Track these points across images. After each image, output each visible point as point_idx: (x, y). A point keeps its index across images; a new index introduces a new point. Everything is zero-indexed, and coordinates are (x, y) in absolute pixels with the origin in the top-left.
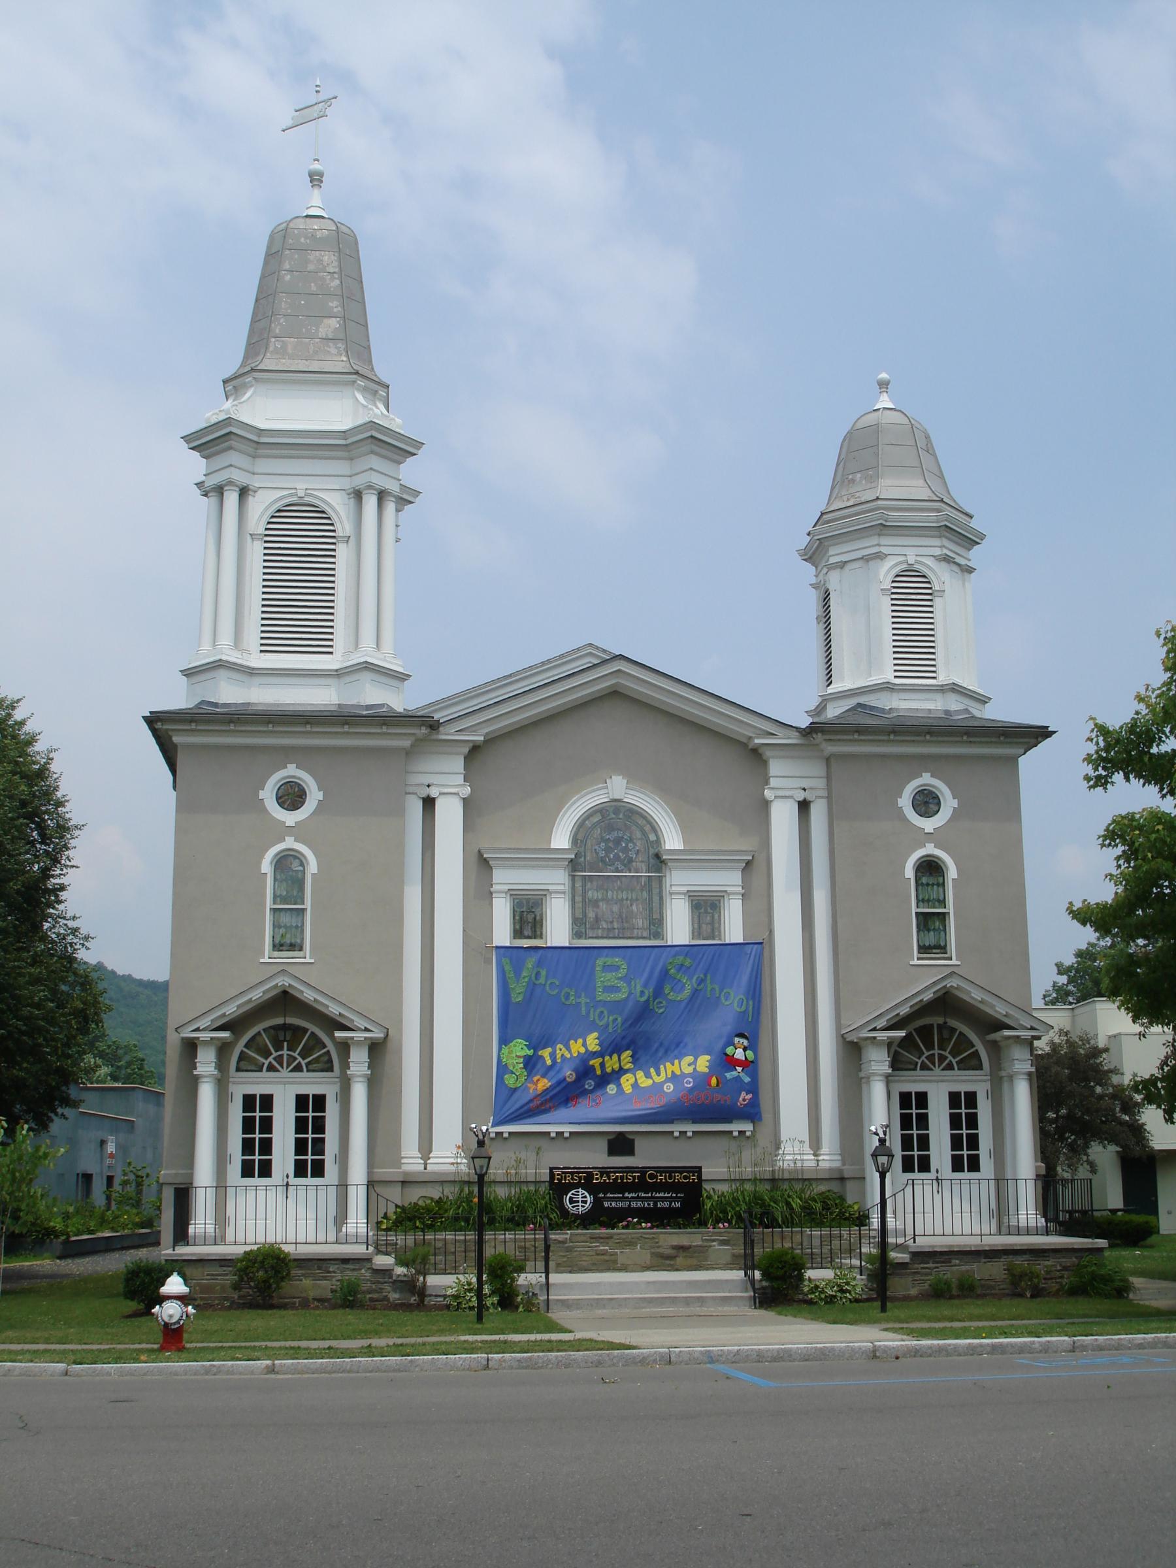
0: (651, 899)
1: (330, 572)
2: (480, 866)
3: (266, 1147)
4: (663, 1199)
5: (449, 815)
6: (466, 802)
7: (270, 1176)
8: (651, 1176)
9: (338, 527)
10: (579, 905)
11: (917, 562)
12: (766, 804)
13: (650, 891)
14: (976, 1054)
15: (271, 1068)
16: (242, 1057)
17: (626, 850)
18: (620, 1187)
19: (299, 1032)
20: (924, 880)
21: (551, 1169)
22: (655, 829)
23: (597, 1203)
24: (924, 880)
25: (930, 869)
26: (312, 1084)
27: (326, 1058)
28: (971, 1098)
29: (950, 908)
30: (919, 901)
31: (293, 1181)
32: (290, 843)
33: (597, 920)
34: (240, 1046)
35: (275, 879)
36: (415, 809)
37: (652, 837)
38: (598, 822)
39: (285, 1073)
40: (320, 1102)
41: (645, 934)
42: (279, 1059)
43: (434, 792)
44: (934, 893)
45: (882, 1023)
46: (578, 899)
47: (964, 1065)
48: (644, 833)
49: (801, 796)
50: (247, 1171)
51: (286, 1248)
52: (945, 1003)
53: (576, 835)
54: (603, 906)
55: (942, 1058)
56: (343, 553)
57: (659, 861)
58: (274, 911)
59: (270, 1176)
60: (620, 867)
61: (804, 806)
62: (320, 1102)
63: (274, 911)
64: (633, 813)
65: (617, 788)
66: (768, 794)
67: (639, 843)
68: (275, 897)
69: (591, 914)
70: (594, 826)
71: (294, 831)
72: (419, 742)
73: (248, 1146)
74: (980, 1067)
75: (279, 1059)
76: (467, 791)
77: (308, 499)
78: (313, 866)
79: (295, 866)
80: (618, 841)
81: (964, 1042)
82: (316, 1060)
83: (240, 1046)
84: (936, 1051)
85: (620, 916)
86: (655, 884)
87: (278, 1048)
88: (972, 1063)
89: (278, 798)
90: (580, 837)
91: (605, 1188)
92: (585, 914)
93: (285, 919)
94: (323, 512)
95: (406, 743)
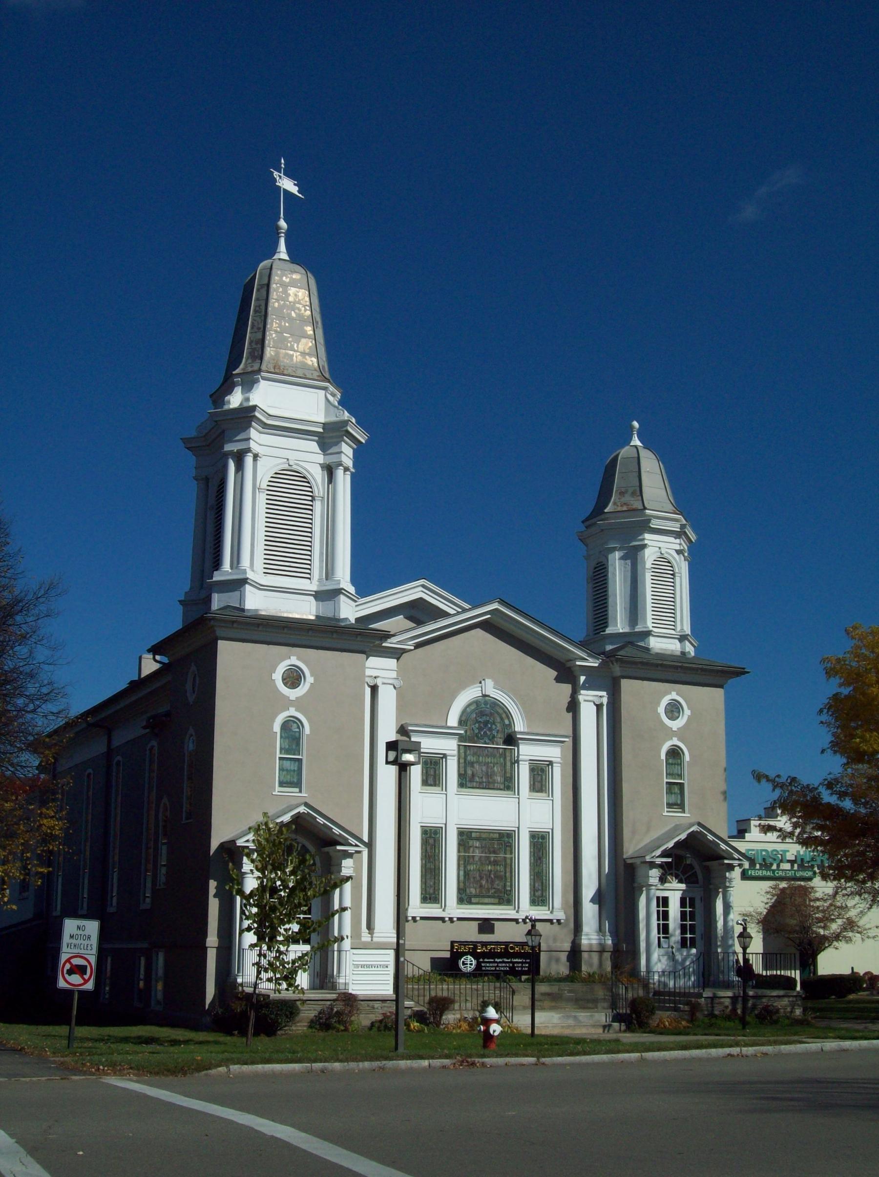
0: (505, 764)
4: (518, 963)
7: (432, 959)
8: (512, 948)
10: (462, 765)
11: (667, 553)
13: (505, 758)
17: (491, 729)
18: (492, 955)
20: (670, 761)
21: (452, 943)
22: (509, 715)
23: (479, 965)
24: (670, 761)
25: (292, 733)
29: (278, 755)
30: (669, 774)
32: (292, 712)
33: (473, 775)
35: (281, 737)
37: (507, 722)
38: (474, 710)
41: (502, 787)
44: (676, 769)
46: (462, 761)
48: (502, 719)
52: (301, 824)
53: (461, 716)
54: (477, 766)
57: (511, 740)
58: (280, 758)
59: (432, 959)
60: (487, 741)
63: (280, 758)
67: (498, 725)
68: (281, 749)
69: (469, 772)
70: (472, 712)
71: (298, 703)
74: (697, 882)
77: (295, 467)
78: (307, 730)
79: (294, 728)
80: (486, 723)
85: (487, 773)
86: (508, 754)
89: (283, 679)
90: (463, 718)
91: (484, 955)
92: (465, 771)
93: (287, 764)
94: (304, 477)
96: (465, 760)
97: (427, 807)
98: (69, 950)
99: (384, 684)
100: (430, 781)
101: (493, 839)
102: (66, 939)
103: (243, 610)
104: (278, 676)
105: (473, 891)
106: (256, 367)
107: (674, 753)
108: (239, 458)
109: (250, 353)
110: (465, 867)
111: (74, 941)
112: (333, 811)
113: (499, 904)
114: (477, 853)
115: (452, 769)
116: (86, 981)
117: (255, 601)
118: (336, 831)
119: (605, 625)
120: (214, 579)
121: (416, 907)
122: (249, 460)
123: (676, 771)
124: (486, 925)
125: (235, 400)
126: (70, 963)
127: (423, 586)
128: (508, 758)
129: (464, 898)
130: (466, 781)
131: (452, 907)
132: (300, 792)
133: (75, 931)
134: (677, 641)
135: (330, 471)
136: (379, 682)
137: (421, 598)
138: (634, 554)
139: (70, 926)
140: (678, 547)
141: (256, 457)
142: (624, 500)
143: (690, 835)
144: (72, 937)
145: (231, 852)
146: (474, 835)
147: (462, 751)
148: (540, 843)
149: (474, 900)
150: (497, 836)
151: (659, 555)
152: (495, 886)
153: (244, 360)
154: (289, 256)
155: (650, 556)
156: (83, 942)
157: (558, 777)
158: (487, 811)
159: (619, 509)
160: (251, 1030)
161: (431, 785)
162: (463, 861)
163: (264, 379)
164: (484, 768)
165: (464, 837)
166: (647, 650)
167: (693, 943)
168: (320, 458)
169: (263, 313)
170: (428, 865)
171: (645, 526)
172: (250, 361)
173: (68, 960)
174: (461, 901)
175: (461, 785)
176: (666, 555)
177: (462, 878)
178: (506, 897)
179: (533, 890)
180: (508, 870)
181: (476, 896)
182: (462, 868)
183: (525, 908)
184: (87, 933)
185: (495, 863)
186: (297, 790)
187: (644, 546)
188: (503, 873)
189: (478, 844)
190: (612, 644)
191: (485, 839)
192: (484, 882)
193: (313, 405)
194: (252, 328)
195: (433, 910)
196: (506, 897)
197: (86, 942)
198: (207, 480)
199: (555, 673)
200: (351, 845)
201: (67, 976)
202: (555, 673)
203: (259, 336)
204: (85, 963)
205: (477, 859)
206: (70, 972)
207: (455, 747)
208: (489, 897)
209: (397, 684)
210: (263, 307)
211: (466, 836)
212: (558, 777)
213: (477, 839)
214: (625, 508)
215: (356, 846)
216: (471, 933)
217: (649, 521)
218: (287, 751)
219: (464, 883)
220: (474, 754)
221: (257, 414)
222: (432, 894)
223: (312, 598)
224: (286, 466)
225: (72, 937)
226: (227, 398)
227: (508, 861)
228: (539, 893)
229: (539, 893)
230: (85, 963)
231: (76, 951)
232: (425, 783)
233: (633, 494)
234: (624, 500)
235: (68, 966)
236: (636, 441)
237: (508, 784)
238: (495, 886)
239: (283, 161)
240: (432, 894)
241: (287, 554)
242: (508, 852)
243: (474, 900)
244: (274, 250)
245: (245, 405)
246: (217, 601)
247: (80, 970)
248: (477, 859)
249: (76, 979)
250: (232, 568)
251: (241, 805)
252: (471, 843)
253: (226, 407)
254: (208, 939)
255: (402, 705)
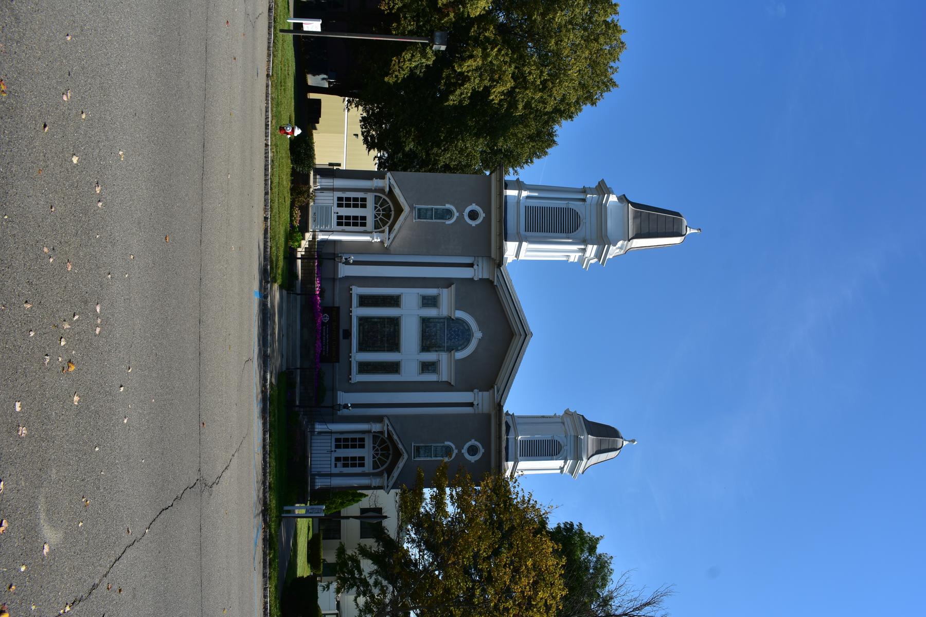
2: (447, 283)
3: (348, 206)
5: (466, 273)
6: (472, 279)
12: (472, 391)
15: (376, 208)
16: (380, 198)
19: (388, 217)
26: (370, 222)
28: (362, 465)
34: (384, 197)
36: (468, 260)
39: (372, 452)
40: (364, 225)
43: (475, 267)
47: (374, 462)
49: (475, 403)
50: (340, 199)
55: (377, 454)
61: (471, 405)
62: (364, 225)
64: (468, 341)
65: (477, 335)
66: (476, 390)
71: (461, 213)
72: (494, 260)
73: (348, 199)
76: (476, 279)
78: (448, 222)
80: (458, 335)
81: (383, 463)
83: (384, 197)
87: (383, 210)
88: (375, 466)
95: (493, 256)
97: (410, 297)
100: (425, 301)
104: (473, 223)
115: (431, 312)
121: (357, 291)
124: (348, 334)
129: (363, 320)
131: (359, 312)
157: (432, 377)
158: (410, 334)
178: (362, 348)
195: (355, 301)
199: (314, 131)
202: (314, 131)
212: (432, 377)
222: (365, 301)
237: (425, 348)
240: (365, 301)
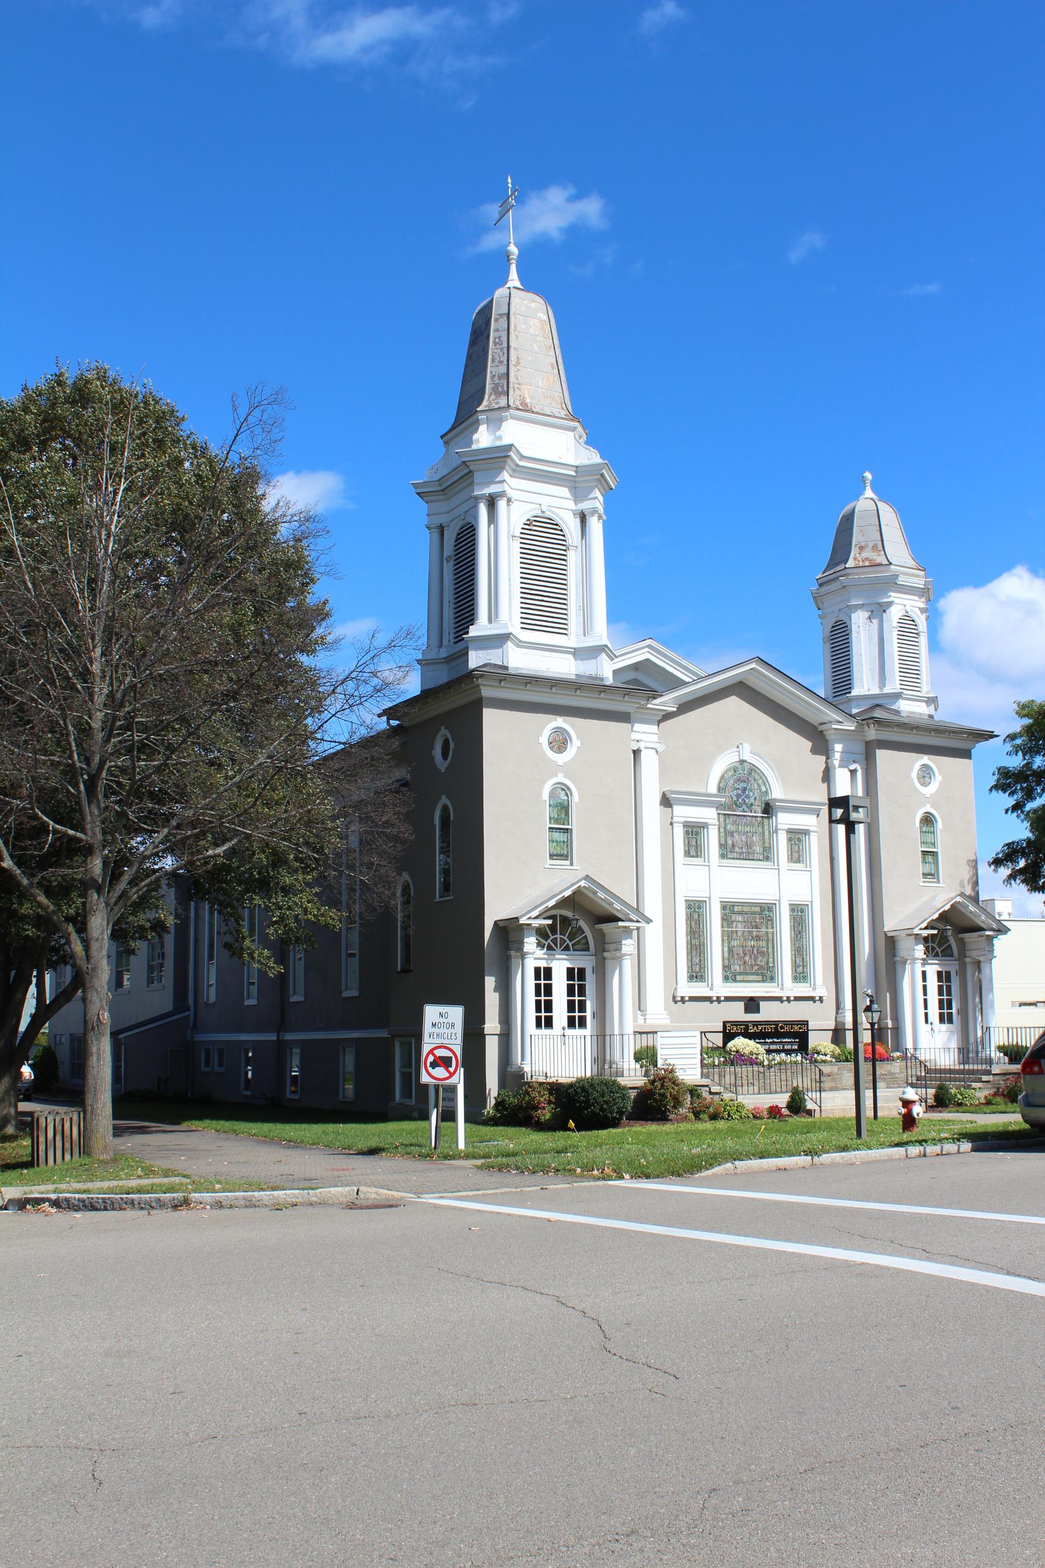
1: (563, 572)
8: (782, 1027)
9: (568, 536)
10: (722, 835)
13: (763, 827)
14: (950, 947)
22: (766, 782)
24: (924, 829)
25: (928, 820)
27: (584, 941)
28: (582, 972)
31: (570, 1032)
33: (733, 846)
37: (764, 789)
42: (555, 941)
44: (929, 838)
45: (924, 925)
46: (722, 830)
48: (759, 786)
51: (561, 1080)
52: (576, 902)
56: (573, 558)
69: (730, 842)
71: (564, 768)
75: (555, 941)
77: (548, 514)
78: (576, 798)
82: (578, 942)
84: (558, 936)
92: (726, 841)
93: (557, 836)
96: (725, 829)
98: (431, 1040)
99: (647, 748)
100: (693, 853)
101: (754, 913)
102: (427, 1028)
103: (506, 668)
105: (737, 967)
106: (503, 402)
107: (928, 820)
108: (492, 503)
109: (493, 389)
110: (729, 943)
111: (436, 1030)
112: (616, 886)
113: (763, 981)
114: (740, 928)
115: (712, 839)
116: (452, 1075)
117: (518, 660)
118: (617, 906)
119: (849, 688)
120: (471, 634)
122: (502, 504)
123: (929, 840)
124: (752, 1004)
125: (483, 438)
126: (434, 1055)
127: (649, 646)
128: (766, 827)
129: (730, 976)
130: (727, 851)
132: (572, 864)
133: (437, 1019)
134: (924, 704)
135: (583, 518)
136: (642, 745)
137: (647, 660)
138: (879, 610)
139: (432, 1013)
140: (922, 605)
141: (509, 501)
142: (865, 555)
143: (952, 906)
144: (434, 1025)
145: (509, 933)
146: (736, 909)
147: (722, 820)
148: (799, 914)
149: (738, 978)
150: (758, 909)
151: (904, 613)
152: (758, 962)
153: (486, 397)
154: (522, 284)
155: (894, 614)
156: (447, 1031)
159: (861, 564)
160: (117, 1122)
161: (693, 856)
162: (728, 936)
163: (514, 418)
164: (744, 838)
165: (727, 911)
166: (897, 712)
167: (582, 1023)
168: (571, 505)
169: (505, 345)
170: (694, 941)
171: (891, 583)
172: (493, 397)
173: (431, 1052)
174: (726, 978)
175: (723, 856)
176: (910, 614)
177: (726, 955)
178: (767, 974)
179: (795, 966)
180: (770, 945)
181: (740, 974)
182: (726, 944)
183: (790, 988)
184: (450, 1020)
185: (758, 938)
186: (568, 863)
187: (891, 604)
188: (765, 949)
189: (740, 918)
190: (858, 706)
191: (746, 913)
192: (747, 958)
193: (563, 446)
194: (493, 360)
196: (767, 974)
197: (450, 1031)
198: (441, 529)
200: (632, 921)
201: (430, 1069)
203: (503, 369)
204: (450, 1054)
205: (740, 934)
206: (434, 1065)
207: (716, 816)
208: (752, 974)
209: (661, 748)
210: (504, 339)
211: (729, 909)
213: (739, 913)
214: (867, 564)
215: (638, 921)
216: (737, 1013)
217: (896, 576)
218: (557, 821)
219: (729, 960)
220: (734, 823)
221: (512, 454)
223: (571, 657)
224: (538, 513)
225: (434, 1025)
226: (475, 437)
227: (770, 936)
228: (800, 969)
229: (800, 969)
230: (450, 1054)
231: (439, 1041)
232: (687, 854)
233: (875, 548)
234: (865, 555)
235: (431, 1058)
236: (869, 493)
237: (767, 855)
238: (758, 962)
239: (509, 180)
241: (545, 606)
242: (770, 926)
243: (738, 978)
244: (504, 279)
245: (498, 443)
246: (475, 659)
247: (445, 1062)
248: (740, 934)
249: (440, 1072)
250: (490, 621)
251: (516, 883)
252: (734, 917)
253: (474, 447)
254: (486, 1026)
255: (664, 771)
